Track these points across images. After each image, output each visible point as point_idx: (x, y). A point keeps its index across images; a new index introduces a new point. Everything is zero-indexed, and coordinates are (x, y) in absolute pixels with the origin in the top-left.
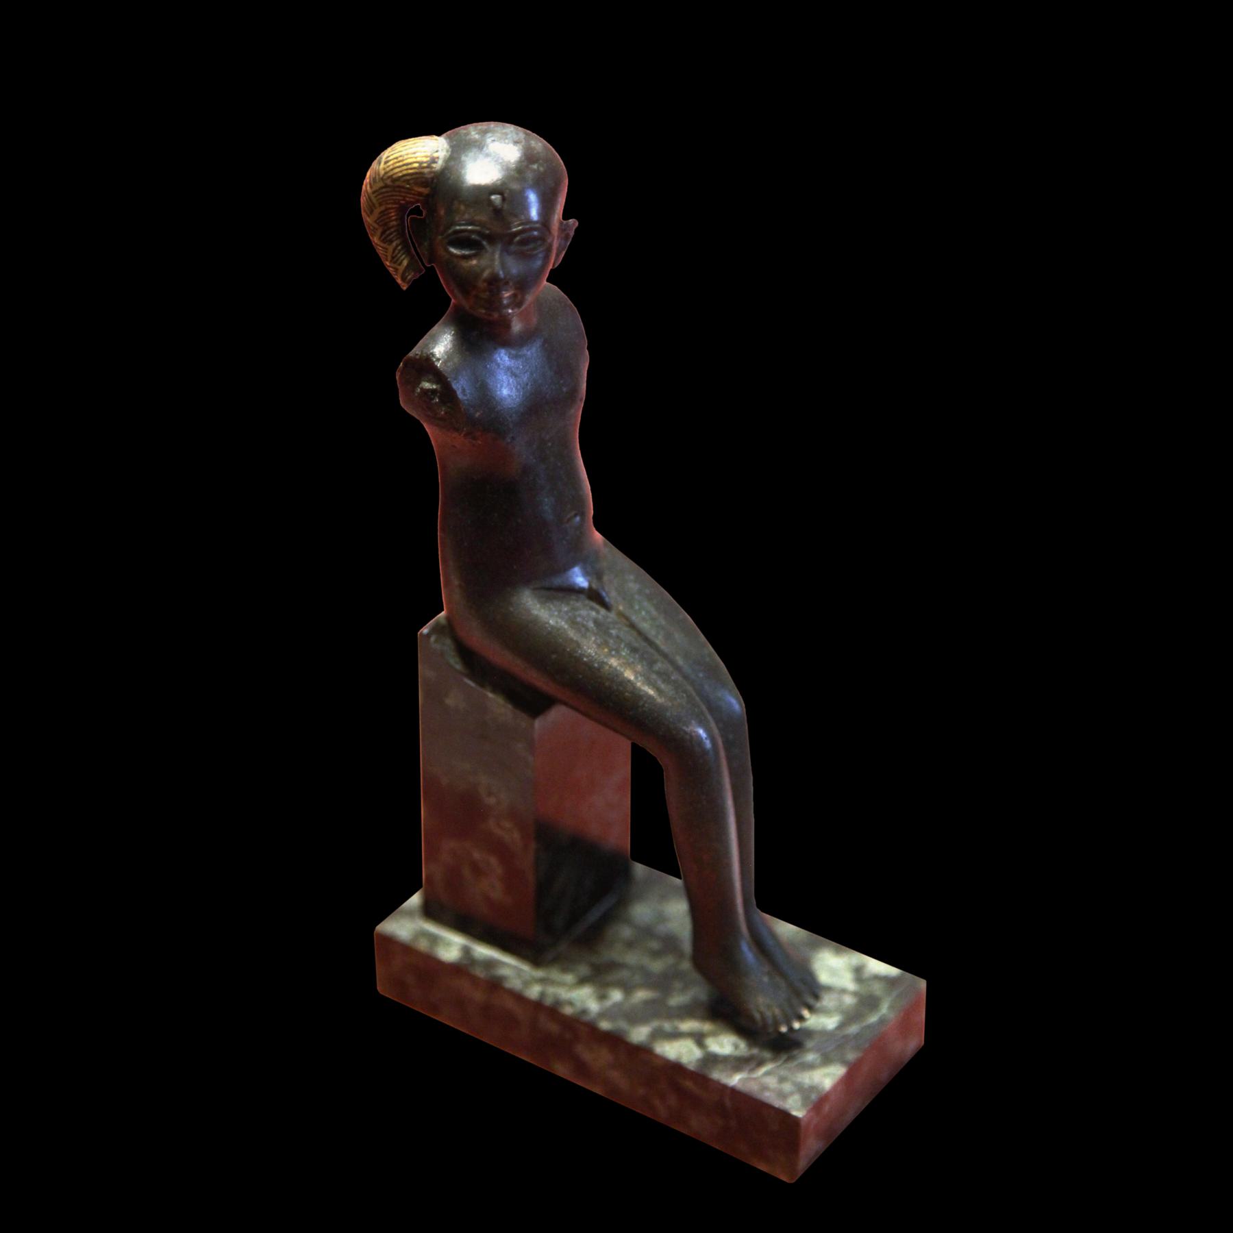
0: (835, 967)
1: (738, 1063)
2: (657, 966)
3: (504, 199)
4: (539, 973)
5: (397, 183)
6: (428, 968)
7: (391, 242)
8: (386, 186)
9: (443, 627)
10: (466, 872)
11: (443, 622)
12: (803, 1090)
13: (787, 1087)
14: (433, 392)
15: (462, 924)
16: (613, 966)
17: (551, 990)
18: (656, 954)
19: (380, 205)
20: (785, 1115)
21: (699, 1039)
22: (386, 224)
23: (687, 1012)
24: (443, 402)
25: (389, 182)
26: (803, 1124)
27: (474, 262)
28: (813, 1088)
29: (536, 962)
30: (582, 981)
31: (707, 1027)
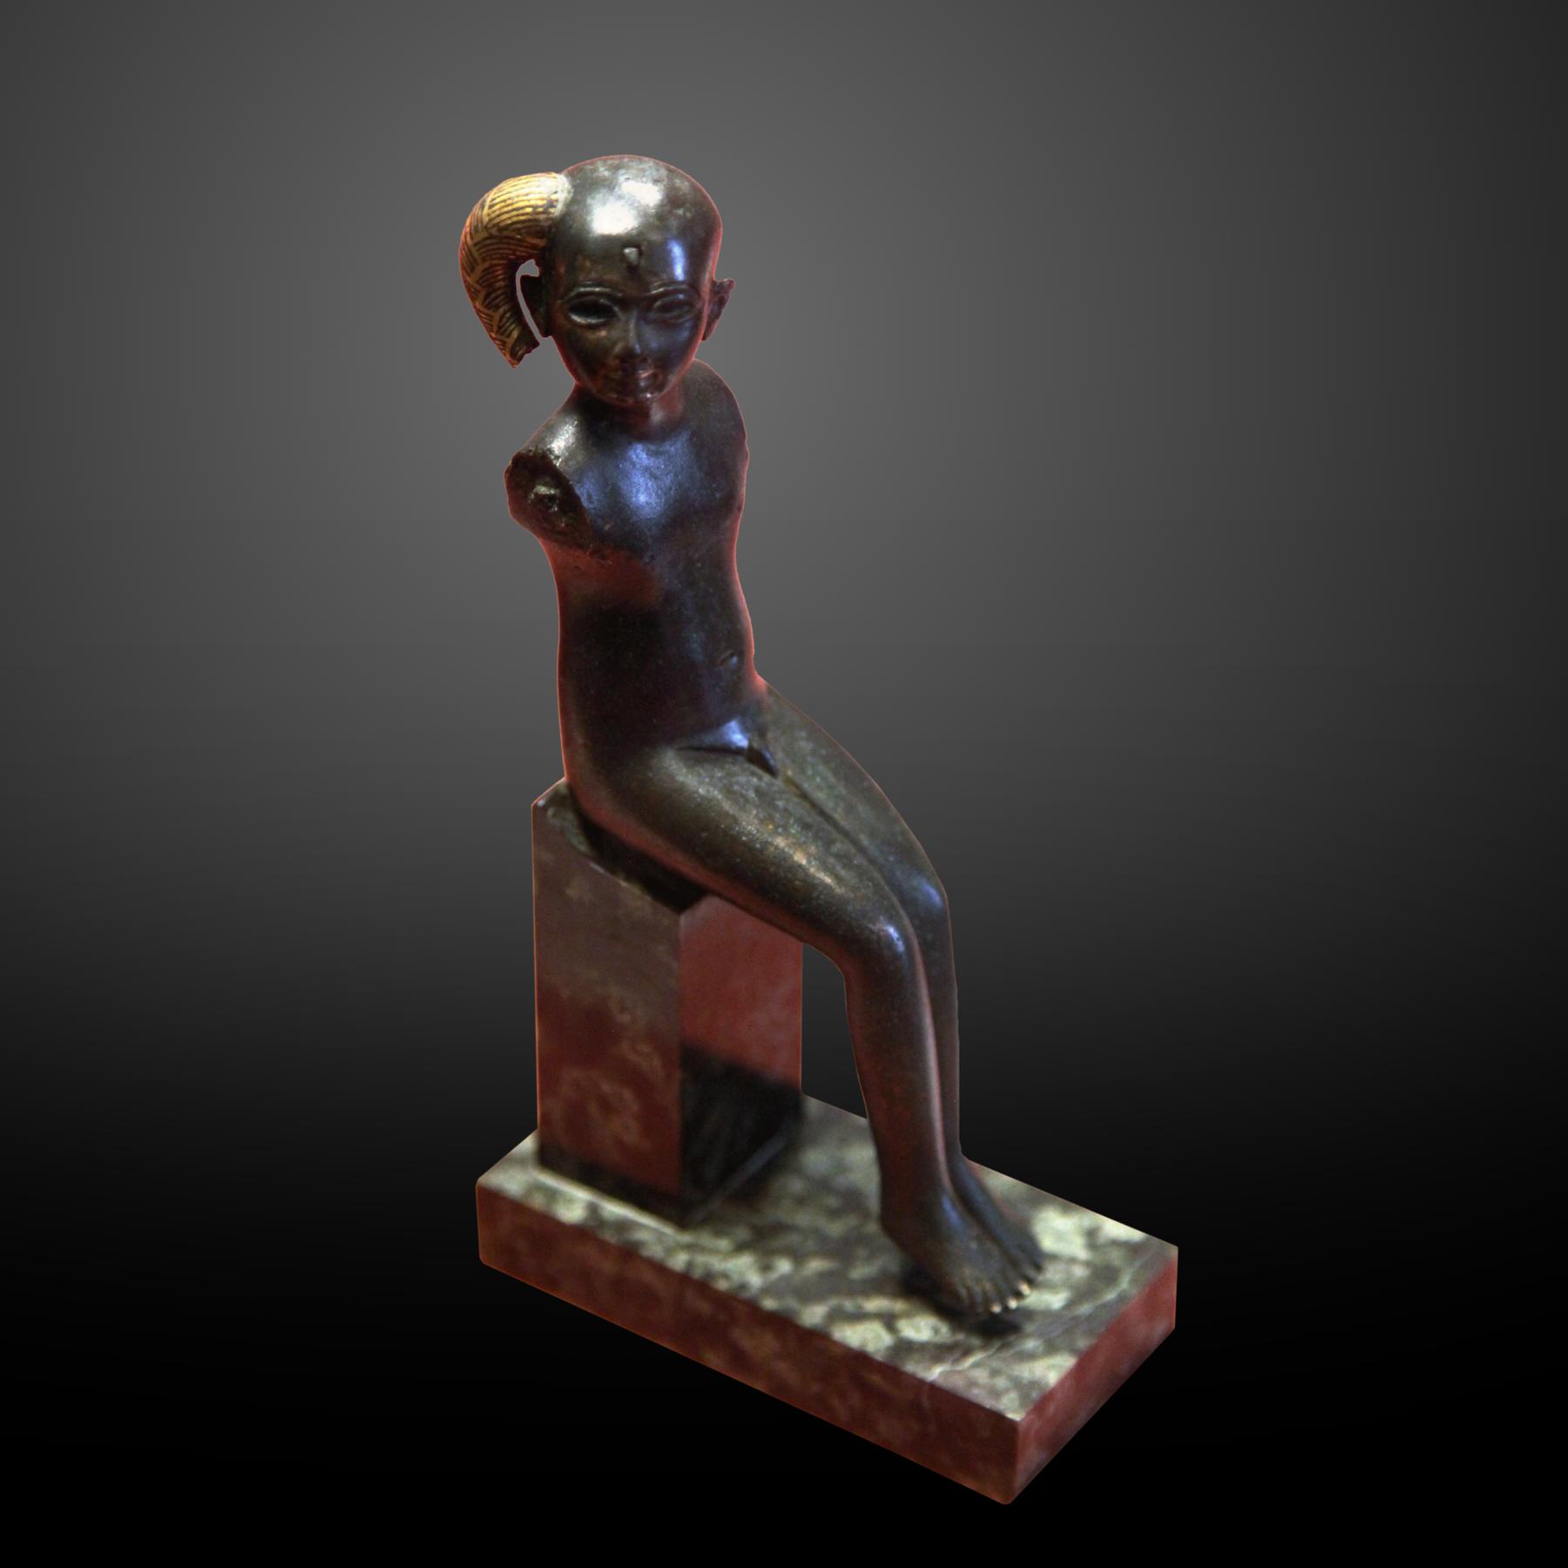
0: (1062, 1230)
1: (938, 1352)
2: (835, 1229)
3: (641, 253)
4: (686, 1238)
5: (505, 233)
6: (544, 1231)
7: (497, 307)
8: (491, 237)
9: (564, 797)
10: (593, 1109)
11: (564, 791)
12: (1021, 1386)
13: (1001, 1382)
14: (551, 498)
15: (588, 1175)
16: (779, 1228)
17: (701, 1259)
18: (834, 1214)
19: (484, 260)
20: (998, 1418)
21: (889, 1321)
22: (490, 285)
23: (874, 1287)
24: (563, 511)
25: (494, 232)
26: (1021, 1429)
27: (603, 333)
28: (1033, 1384)
29: (682, 1223)
30: (740, 1248)
31: (899, 1306)
